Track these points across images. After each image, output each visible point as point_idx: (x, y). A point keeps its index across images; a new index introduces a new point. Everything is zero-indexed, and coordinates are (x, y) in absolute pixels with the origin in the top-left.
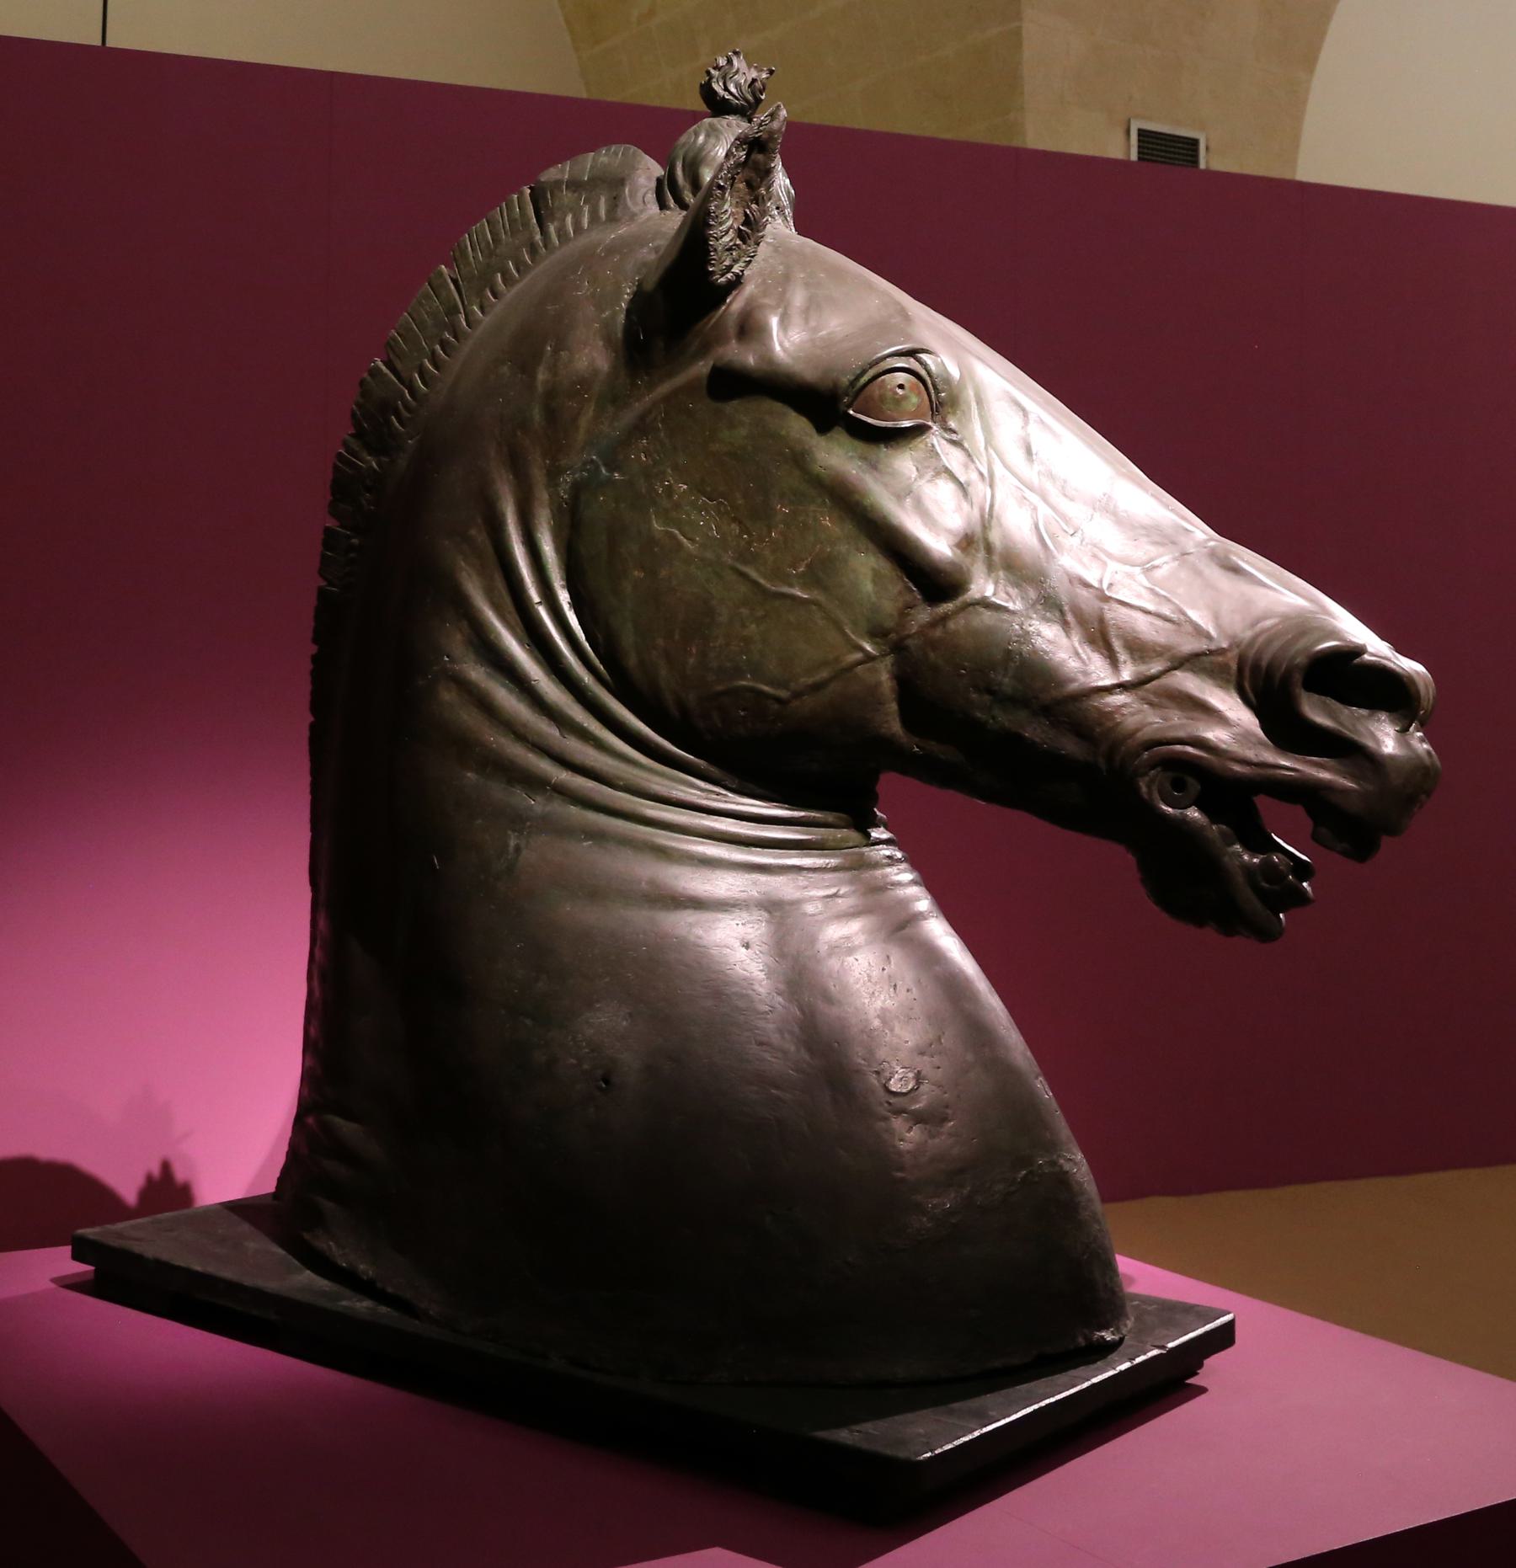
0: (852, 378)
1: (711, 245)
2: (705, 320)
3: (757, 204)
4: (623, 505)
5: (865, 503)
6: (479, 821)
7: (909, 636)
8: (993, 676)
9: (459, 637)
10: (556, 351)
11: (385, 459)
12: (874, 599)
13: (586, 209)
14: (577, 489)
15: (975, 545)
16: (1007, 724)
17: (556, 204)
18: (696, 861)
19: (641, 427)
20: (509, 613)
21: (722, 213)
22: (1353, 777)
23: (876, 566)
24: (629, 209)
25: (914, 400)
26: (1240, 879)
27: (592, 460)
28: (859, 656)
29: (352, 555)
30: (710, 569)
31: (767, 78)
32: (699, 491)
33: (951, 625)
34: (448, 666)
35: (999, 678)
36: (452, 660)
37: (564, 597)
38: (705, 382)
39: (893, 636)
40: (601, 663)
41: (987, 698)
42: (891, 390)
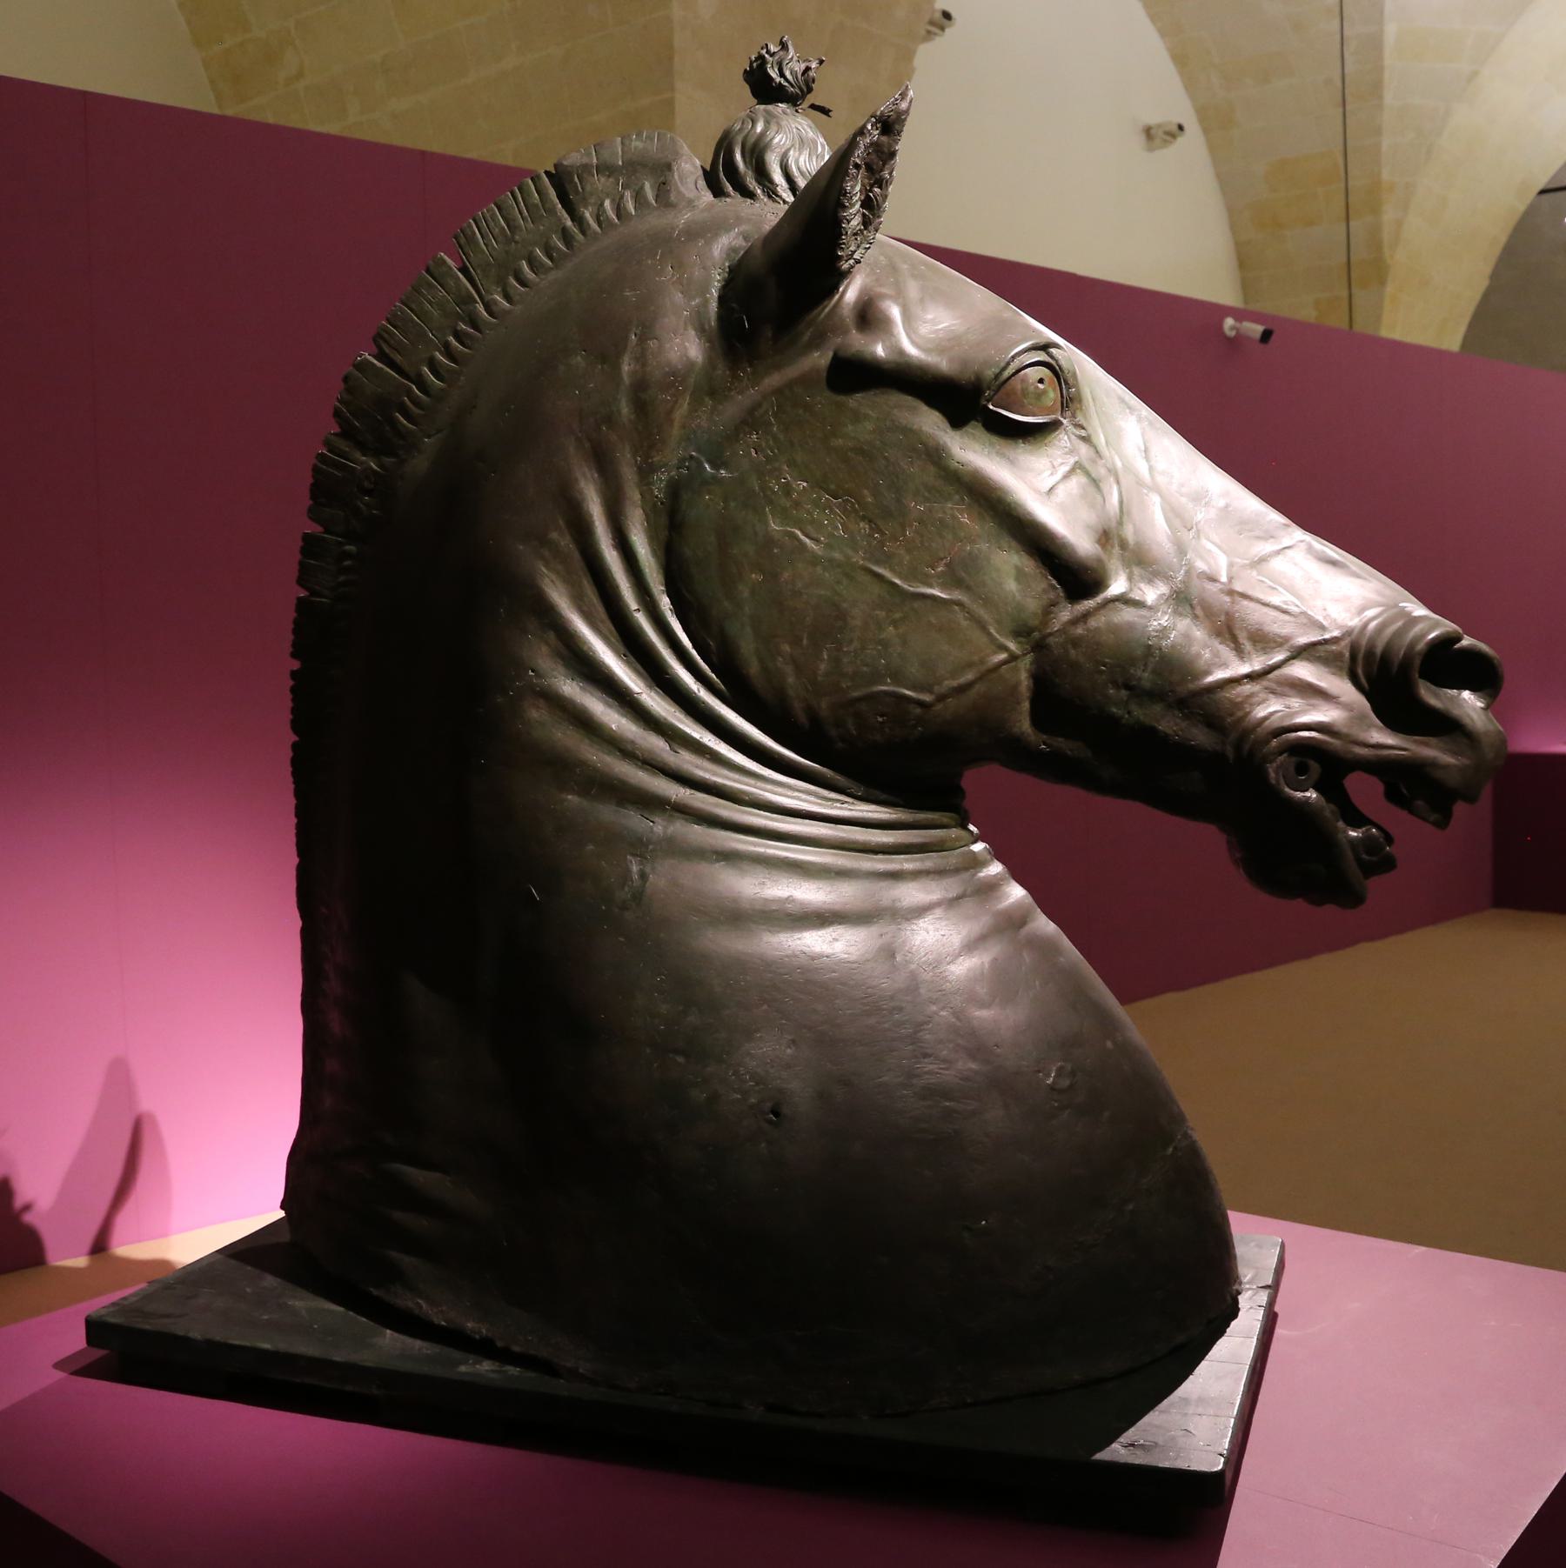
0: (997, 371)
2: (816, 312)
3: (880, 187)
4: (732, 504)
6: (590, 847)
7: (1051, 634)
8: (1132, 671)
9: (544, 649)
10: (643, 339)
11: (388, 460)
12: (1018, 597)
13: (628, 194)
14: (674, 490)
16: (1142, 718)
17: (588, 188)
18: (833, 874)
19: (750, 421)
20: (602, 622)
22: (1454, 753)
23: (1019, 564)
24: (684, 195)
25: (1052, 395)
27: (692, 457)
28: (1003, 656)
29: (347, 563)
30: (839, 570)
31: (817, 68)
32: (821, 488)
33: (1093, 623)
35: (1139, 673)
36: (538, 675)
37: (665, 603)
38: (824, 374)
39: (1036, 634)
40: (713, 672)
41: (1124, 693)
42: (1033, 384)
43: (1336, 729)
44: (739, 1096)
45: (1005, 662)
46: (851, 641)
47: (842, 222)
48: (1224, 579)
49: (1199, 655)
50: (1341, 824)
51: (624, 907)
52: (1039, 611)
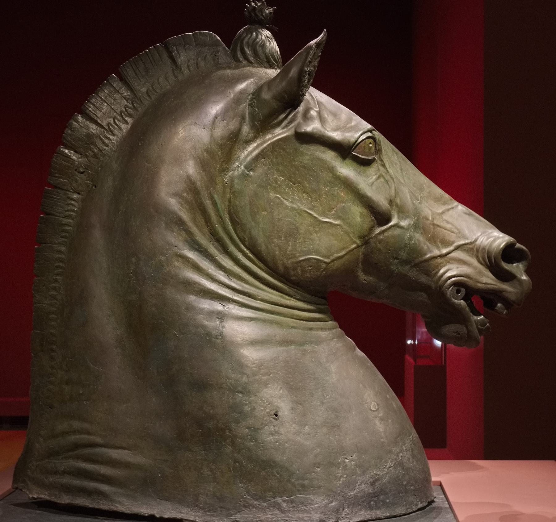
5: (358, 187)
7: (371, 238)
26: (474, 322)
30: (296, 211)
32: (289, 180)
35: (402, 254)
39: (366, 238)
43: (471, 277)
44: (263, 409)
45: (355, 248)
46: (300, 238)
48: (430, 219)
49: (423, 248)
50: (471, 314)
51: (216, 338)
52: (368, 229)
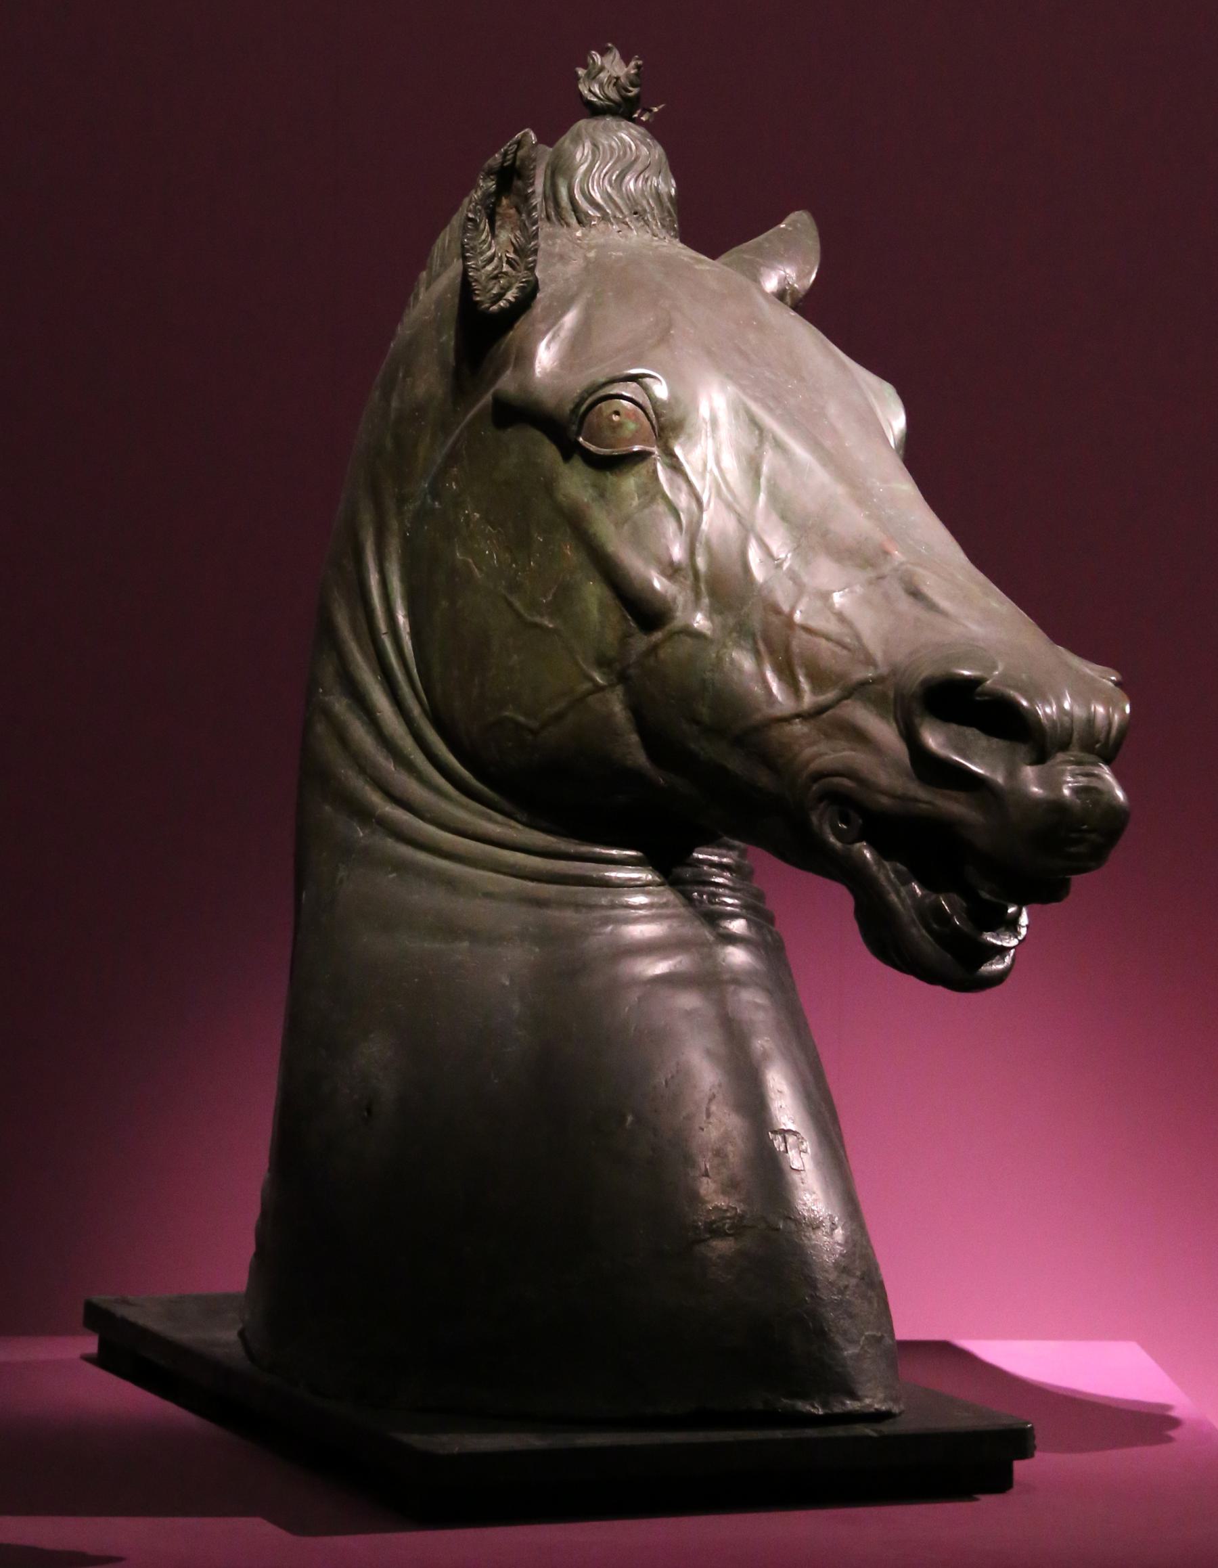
0: (571, 406)
1: (471, 276)
15: (683, 573)
21: (480, 244)
28: (587, 686)
34: (321, 697)
39: (618, 666)
45: (591, 693)
47: (424, 269)
